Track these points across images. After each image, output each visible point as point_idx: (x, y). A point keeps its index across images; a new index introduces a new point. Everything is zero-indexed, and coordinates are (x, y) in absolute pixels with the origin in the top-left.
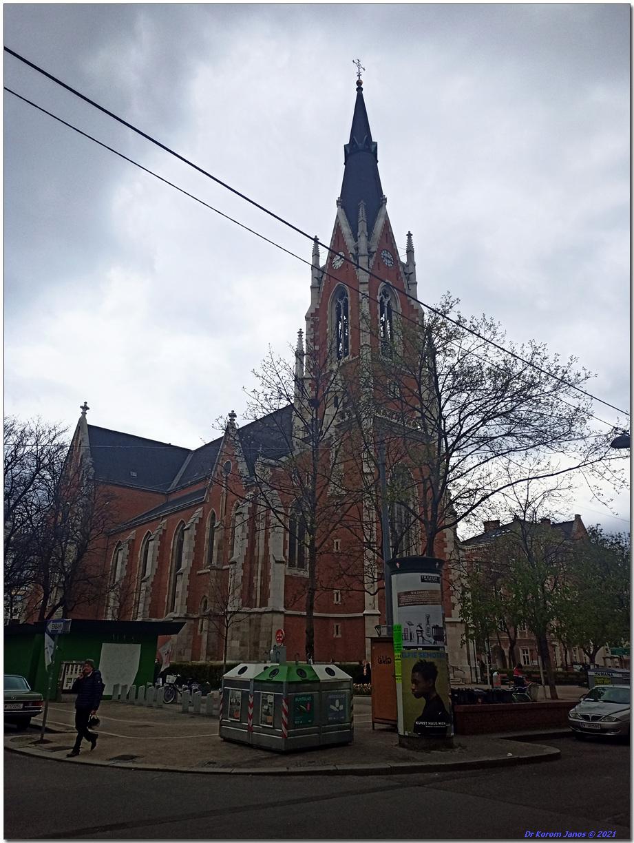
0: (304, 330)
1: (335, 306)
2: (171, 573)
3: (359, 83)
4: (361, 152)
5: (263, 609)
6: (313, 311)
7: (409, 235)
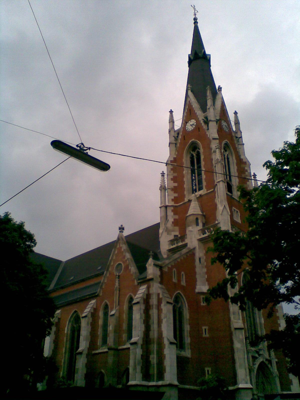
0: (165, 172)
1: (189, 156)
2: (65, 353)
3: (195, 19)
4: (199, 60)
5: (160, 383)
6: (172, 159)
7: (171, 112)
